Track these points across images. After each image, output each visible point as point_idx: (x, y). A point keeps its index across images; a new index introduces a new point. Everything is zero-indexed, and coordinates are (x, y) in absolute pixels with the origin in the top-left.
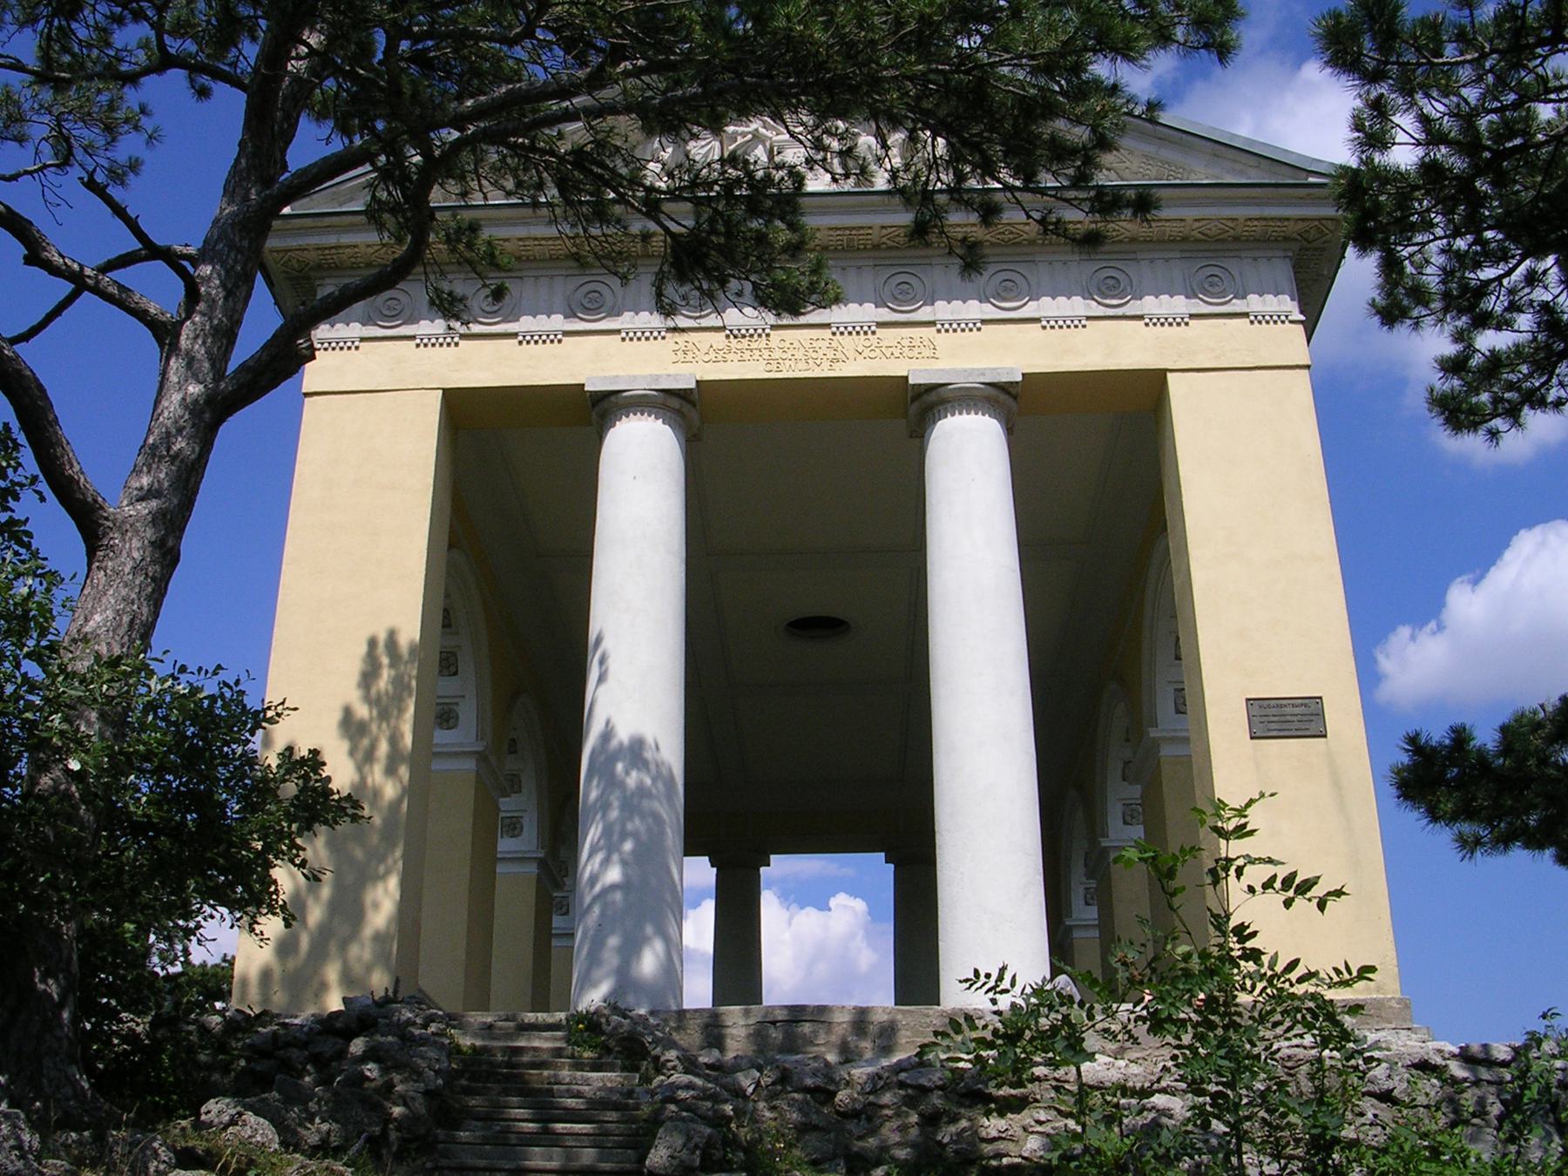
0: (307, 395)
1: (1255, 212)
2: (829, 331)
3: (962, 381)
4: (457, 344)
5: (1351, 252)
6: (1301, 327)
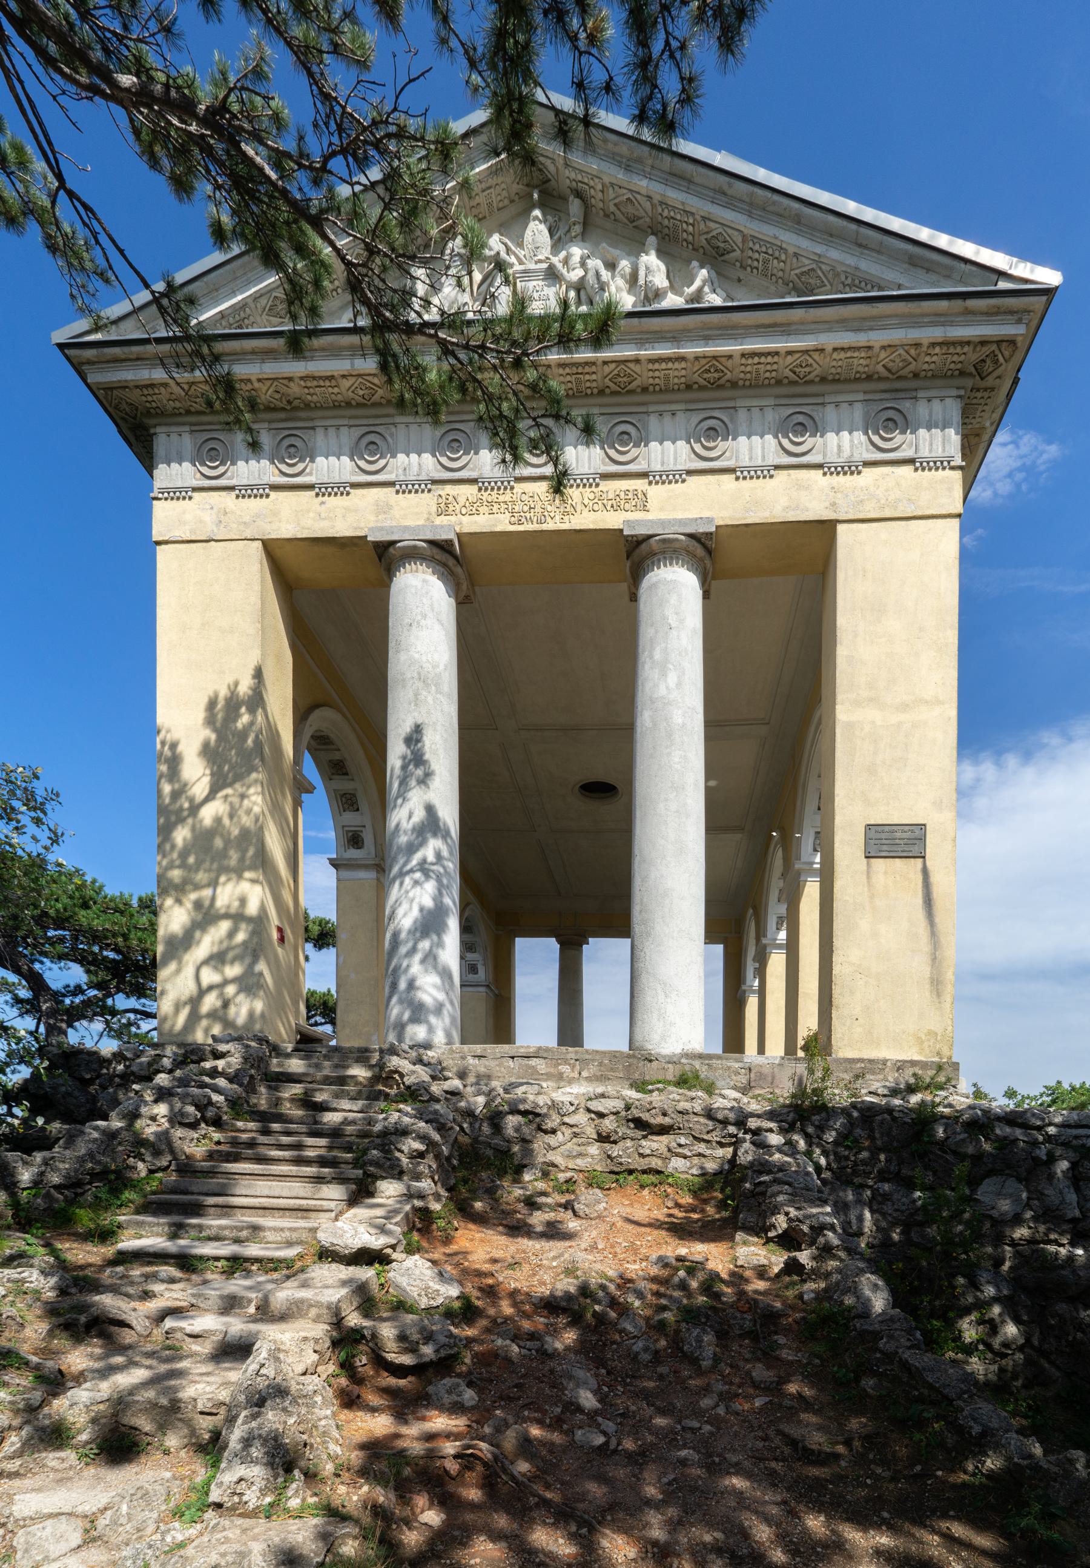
0: (158, 543)
1: (937, 333)
2: (476, 487)
3: (669, 533)
4: (268, 496)
5: (333, 918)
6: (958, 474)
